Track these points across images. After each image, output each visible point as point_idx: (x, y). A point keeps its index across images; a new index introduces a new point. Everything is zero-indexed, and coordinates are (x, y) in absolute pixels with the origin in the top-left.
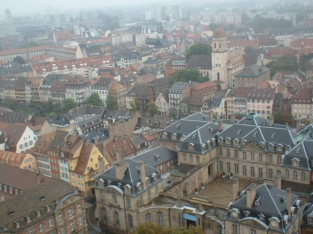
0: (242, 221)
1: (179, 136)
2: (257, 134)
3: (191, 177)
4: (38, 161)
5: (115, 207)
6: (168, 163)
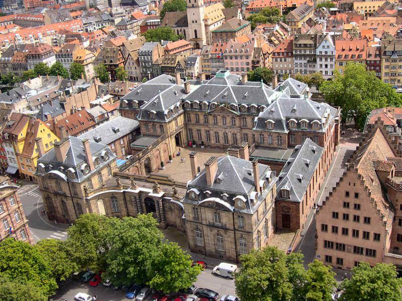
0: (203, 203)
1: (141, 103)
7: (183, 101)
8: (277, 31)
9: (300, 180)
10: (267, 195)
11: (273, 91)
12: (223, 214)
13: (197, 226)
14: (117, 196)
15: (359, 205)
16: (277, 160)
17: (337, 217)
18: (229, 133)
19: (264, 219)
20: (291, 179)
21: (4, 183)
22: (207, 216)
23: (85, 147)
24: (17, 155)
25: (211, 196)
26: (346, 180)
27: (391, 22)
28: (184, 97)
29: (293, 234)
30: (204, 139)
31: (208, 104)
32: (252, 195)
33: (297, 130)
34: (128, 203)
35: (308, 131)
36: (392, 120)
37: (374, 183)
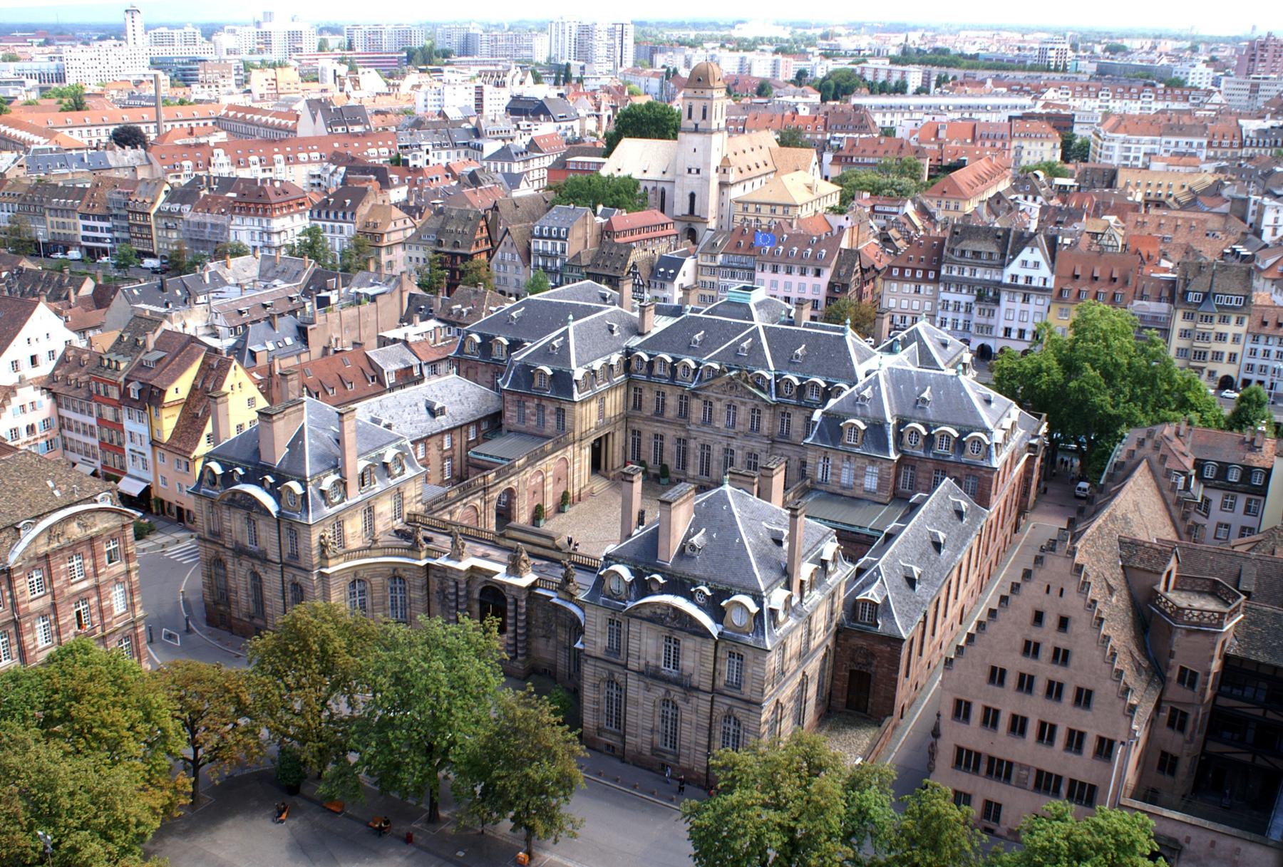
0: (638, 607)
2: (751, 348)
3: (530, 471)
4: (66, 413)
5: (667, 680)
6: (472, 430)
7: (629, 352)
8: (906, 215)
9: (911, 582)
10: (817, 608)
11: (875, 351)
12: (689, 644)
13: (611, 673)
14: (406, 575)
15: (1066, 653)
16: (857, 529)
17: (1001, 682)
18: (740, 452)
19: (799, 676)
20: (889, 575)
21: (98, 498)
22: (643, 648)
23: (342, 429)
24: (155, 443)
25: (664, 590)
26: (1041, 577)
27: (1210, 225)
28: (635, 341)
29: (876, 729)
30: (670, 460)
31: (693, 366)
32: (777, 598)
33: (921, 453)
34: (434, 598)
35: (952, 458)
36: (1182, 458)
37: (1114, 599)
